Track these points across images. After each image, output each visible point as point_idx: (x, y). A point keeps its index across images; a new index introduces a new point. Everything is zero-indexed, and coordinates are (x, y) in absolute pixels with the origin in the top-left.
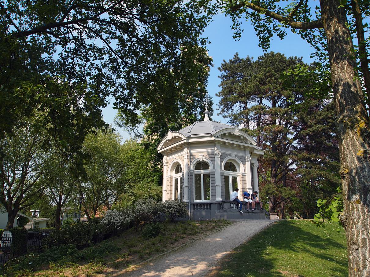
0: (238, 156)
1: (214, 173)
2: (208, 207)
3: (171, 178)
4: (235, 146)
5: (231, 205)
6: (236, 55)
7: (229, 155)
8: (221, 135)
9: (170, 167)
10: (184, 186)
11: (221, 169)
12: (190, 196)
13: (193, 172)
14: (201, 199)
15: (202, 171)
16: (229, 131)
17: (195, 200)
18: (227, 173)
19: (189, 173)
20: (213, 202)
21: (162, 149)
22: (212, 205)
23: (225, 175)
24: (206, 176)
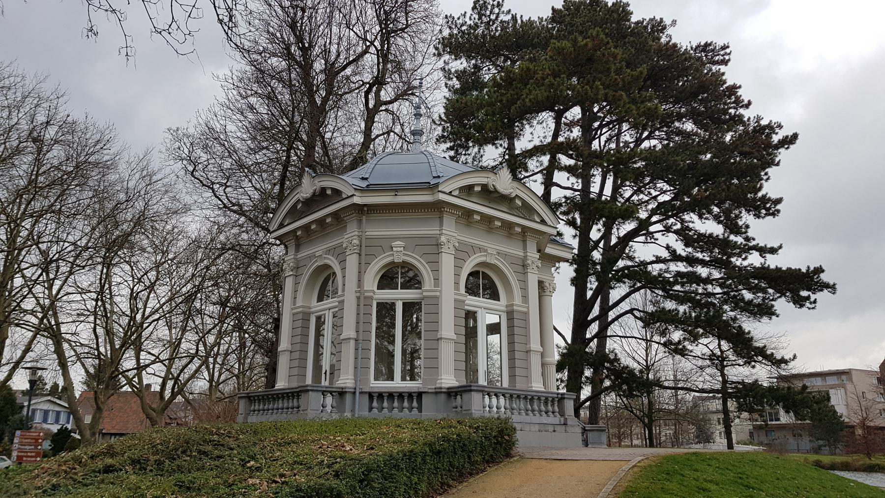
0: (505, 256)
1: (435, 301)
2: (415, 404)
3: (304, 313)
4: (477, 217)
5: (483, 398)
6: (553, 8)
7: (480, 249)
8: (461, 189)
9: (304, 280)
10: (342, 337)
11: (457, 284)
12: (359, 369)
13: (371, 294)
14: (391, 377)
15: (399, 296)
16: (484, 181)
17: (376, 379)
18: (473, 302)
19: (358, 298)
20: (430, 387)
21: (281, 226)
22: (424, 396)
23: (466, 307)
24: (410, 308)
